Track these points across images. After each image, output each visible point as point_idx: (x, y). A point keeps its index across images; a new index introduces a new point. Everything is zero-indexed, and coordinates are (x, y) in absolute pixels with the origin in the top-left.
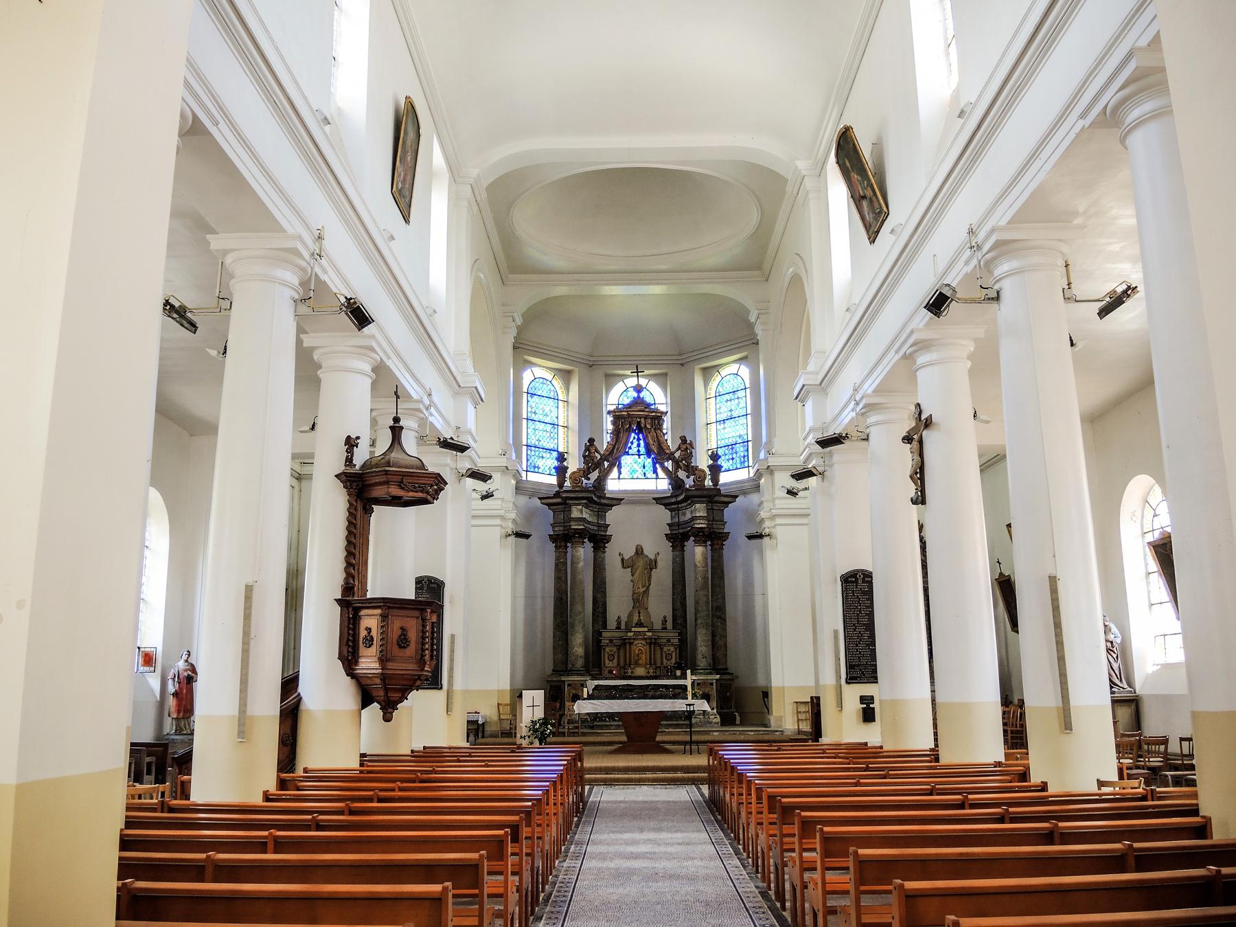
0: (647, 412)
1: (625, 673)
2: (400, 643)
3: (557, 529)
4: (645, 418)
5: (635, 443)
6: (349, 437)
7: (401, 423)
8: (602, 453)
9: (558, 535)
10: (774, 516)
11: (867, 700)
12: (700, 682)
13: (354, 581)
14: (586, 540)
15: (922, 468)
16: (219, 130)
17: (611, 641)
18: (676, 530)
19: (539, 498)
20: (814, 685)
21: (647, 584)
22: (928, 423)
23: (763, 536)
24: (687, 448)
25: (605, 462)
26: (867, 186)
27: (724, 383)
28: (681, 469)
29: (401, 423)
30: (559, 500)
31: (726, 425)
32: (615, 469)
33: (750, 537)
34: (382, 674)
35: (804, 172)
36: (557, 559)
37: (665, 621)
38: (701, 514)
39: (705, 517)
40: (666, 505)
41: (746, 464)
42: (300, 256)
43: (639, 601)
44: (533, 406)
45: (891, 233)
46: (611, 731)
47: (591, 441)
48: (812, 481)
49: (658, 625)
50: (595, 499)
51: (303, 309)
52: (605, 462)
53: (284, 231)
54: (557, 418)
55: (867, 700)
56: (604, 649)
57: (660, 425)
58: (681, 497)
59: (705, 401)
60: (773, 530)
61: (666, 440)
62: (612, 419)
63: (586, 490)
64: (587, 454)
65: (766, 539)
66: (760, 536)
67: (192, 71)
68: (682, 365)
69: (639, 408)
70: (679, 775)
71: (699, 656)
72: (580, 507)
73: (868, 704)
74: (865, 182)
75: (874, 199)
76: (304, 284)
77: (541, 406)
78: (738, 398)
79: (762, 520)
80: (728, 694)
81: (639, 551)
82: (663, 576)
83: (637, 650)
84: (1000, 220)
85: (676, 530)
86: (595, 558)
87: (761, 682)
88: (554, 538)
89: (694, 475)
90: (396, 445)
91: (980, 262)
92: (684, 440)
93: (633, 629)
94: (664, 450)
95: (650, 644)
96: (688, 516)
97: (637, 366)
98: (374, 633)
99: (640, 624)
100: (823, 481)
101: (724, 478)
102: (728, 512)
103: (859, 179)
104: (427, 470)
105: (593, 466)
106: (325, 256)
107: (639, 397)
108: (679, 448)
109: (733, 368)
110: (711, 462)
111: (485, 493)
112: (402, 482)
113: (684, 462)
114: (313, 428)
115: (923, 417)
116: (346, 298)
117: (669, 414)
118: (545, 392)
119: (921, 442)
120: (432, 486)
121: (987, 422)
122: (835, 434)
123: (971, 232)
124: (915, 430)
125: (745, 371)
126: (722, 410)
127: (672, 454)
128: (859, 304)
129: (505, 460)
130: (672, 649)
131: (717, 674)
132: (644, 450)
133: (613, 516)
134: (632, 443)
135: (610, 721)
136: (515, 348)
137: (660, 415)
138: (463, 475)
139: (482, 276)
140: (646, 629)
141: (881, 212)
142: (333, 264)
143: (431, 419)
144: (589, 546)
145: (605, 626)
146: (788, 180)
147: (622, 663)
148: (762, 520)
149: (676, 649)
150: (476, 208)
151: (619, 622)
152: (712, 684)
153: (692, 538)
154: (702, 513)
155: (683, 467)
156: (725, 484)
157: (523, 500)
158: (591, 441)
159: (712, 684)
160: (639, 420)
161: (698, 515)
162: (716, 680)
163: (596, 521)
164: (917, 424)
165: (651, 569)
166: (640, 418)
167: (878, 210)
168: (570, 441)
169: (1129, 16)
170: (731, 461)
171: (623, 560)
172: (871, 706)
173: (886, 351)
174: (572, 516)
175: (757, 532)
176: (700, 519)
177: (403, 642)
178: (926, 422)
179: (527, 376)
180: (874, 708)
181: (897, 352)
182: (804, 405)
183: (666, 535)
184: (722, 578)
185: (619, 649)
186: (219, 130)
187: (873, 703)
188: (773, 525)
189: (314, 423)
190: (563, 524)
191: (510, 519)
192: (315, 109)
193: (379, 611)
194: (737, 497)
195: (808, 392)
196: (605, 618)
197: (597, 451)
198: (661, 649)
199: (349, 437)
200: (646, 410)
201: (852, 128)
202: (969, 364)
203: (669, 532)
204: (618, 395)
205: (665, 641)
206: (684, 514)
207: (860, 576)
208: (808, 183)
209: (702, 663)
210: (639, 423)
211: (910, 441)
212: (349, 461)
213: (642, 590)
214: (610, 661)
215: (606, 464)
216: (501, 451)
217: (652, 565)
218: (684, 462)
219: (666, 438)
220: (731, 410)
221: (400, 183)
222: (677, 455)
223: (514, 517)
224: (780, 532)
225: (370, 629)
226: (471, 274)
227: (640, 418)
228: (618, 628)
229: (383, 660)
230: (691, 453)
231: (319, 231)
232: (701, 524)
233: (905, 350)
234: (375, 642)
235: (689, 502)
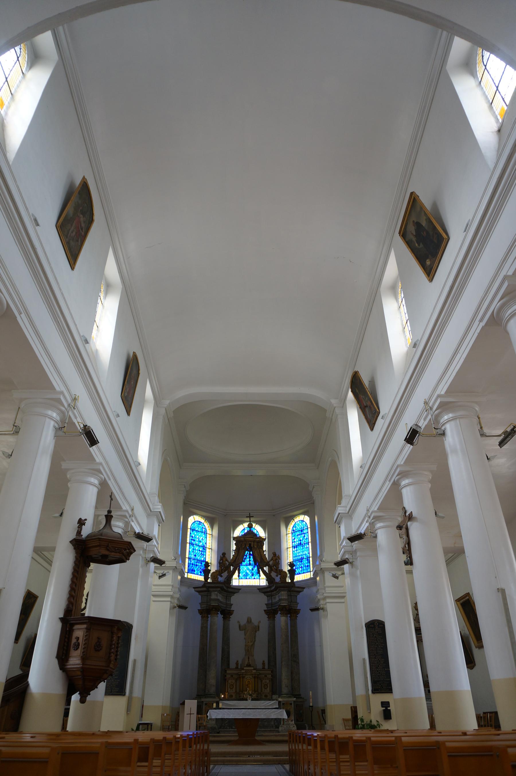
0: (255, 538)
1: (239, 697)
2: (96, 647)
3: (203, 606)
4: (254, 542)
5: (248, 559)
6: (80, 519)
7: (112, 514)
8: (230, 561)
9: (203, 610)
10: (325, 597)
11: (385, 705)
12: (284, 702)
13: (72, 606)
14: (219, 613)
15: (409, 543)
16: (21, 317)
17: (232, 676)
18: (270, 607)
19: (194, 588)
20: (352, 703)
21: (254, 640)
22: (410, 517)
23: (319, 609)
24: (276, 559)
25: (231, 567)
26: (368, 400)
27: (296, 526)
28: (273, 571)
29: (112, 514)
30: (204, 589)
31: (298, 549)
32: (237, 572)
33: (312, 610)
34: (82, 668)
35: (335, 405)
36: (202, 624)
37: (264, 664)
38: (285, 598)
39: (286, 599)
40: (264, 593)
41: (309, 570)
42: (63, 405)
43: (249, 650)
44: (193, 536)
45: (382, 418)
46: (230, 734)
47: (224, 554)
48: (346, 567)
49: (260, 666)
50: (225, 588)
51: (60, 433)
52: (231, 567)
53: (55, 389)
54: (206, 543)
55: (385, 705)
56: (228, 681)
57: (261, 546)
58: (273, 588)
59: (286, 550)
60: (325, 606)
61: (265, 555)
62: (235, 542)
63: (220, 583)
64: (221, 562)
65: (321, 611)
66: (317, 609)
67: (11, 284)
68: (274, 515)
69: (250, 536)
70: (271, 758)
71: (283, 686)
72: (216, 593)
73: (386, 708)
74: (367, 398)
75: (372, 406)
76: (63, 421)
77: (197, 537)
78: (304, 533)
79: (319, 600)
80: (301, 711)
81: (249, 621)
82: (262, 636)
83: (247, 682)
84: (441, 392)
85: (270, 607)
86: (224, 624)
87: (321, 705)
88: (201, 612)
89: (280, 575)
90: (107, 526)
91: (432, 416)
92: (275, 554)
93: (245, 668)
94: (264, 560)
95: (255, 677)
96: (277, 599)
97: (250, 514)
98: (80, 641)
99: (249, 665)
100: (352, 568)
101: (297, 578)
102: (300, 597)
103: (363, 397)
104: (124, 540)
105: (225, 569)
106: (76, 409)
107: (250, 530)
108: (272, 559)
109: (301, 517)
110: (289, 568)
111: (161, 575)
112: (108, 546)
113: (275, 567)
114: (61, 515)
115: (407, 514)
116: (84, 425)
117: (267, 540)
118: (200, 529)
119: (407, 529)
120: (125, 550)
121: (443, 517)
122: (358, 533)
123: (426, 403)
124: (404, 521)
125: (307, 519)
126: (295, 540)
127: (268, 562)
128: (366, 463)
129: (175, 563)
130: (268, 681)
131: (294, 698)
132: (252, 559)
133: (234, 599)
134: (246, 556)
135: (229, 729)
136: (185, 504)
137: (261, 540)
138: (148, 561)
139: (168, 458)
140: (252, 668)
141: (375, 413)
142: (82, 417)
143: (133, 524)
144: (220, 617)
145: (228, 665)
146: (326, 410)
147: (238, 691)
148: (319, 600)
149: (270, 681)
150: (167, 421)
151: (237, 664)
152: (291, 704)
153: (279, 612)
154: (285, 597)
155: (274, 570)
156: (298, 582)
157: (184, 589)
158: (224, 554)
159: (291, 704)
160: (250, 543)
161: (282, 598)
162: (294, 701)
163: (225, 602)
164: (404, 519)
165: (256, 631)
166: (251, 542)
167: (374, 411)
168: (212, 557)
169: (501, 263)
170: (301, 569)
171: (240, 626)
172: (388, 708)
173: (384, 484)
174: (212, 598)
175: (316, 607)
176: (284, 600)
177: (98, 647)
178: (409, 516)
179: (191, 520)
180: (390, 710)
181: (390, 481)
182: (340, 527)
183: (265, 611)
184: (296, 636)
185: (236, 681)
186: (21, 317)
187: (389, 707)
188: (325, 603)
189: (62, 512)
190: (206, 603)
191: (176, 598)
192: (81, 335)
193: (85, 626)
194: (304, 588)
195: (342, 518)
196: (229, 661)
197: (227, 560)
198: (262, 681)
199: (80, 519)
200: (254, 537)
201: (359, 372)
202: (430, 485)
203: (266, 609)
204: (239, 531)
205: (263, 676)
206: (275, 598)
207: (376, 624)
208: (337, 411)
209: (285, 690)
210: (250, 545)
211: (401, 528)
212: (79, 533)
213: (250, 644)
214: (231, 689)
215: (232, 568)
216: (173, 557)
217: (257, 628)
218: (275, 567)
219: (265, 553)
220: (300, 540)
221: (126, 393)
222: (271, 563)
223: (178, 597)
224: (330, 607)
225: (78, 638)
226: (162, 456)
227: (251, 542)
228: (237, 668)
229: (84, 658)
230: (279, 561)
231: (75, 396)
232: (284, 604)
233: (394, 478)
234: (80, 647)
235: (278, 590)
